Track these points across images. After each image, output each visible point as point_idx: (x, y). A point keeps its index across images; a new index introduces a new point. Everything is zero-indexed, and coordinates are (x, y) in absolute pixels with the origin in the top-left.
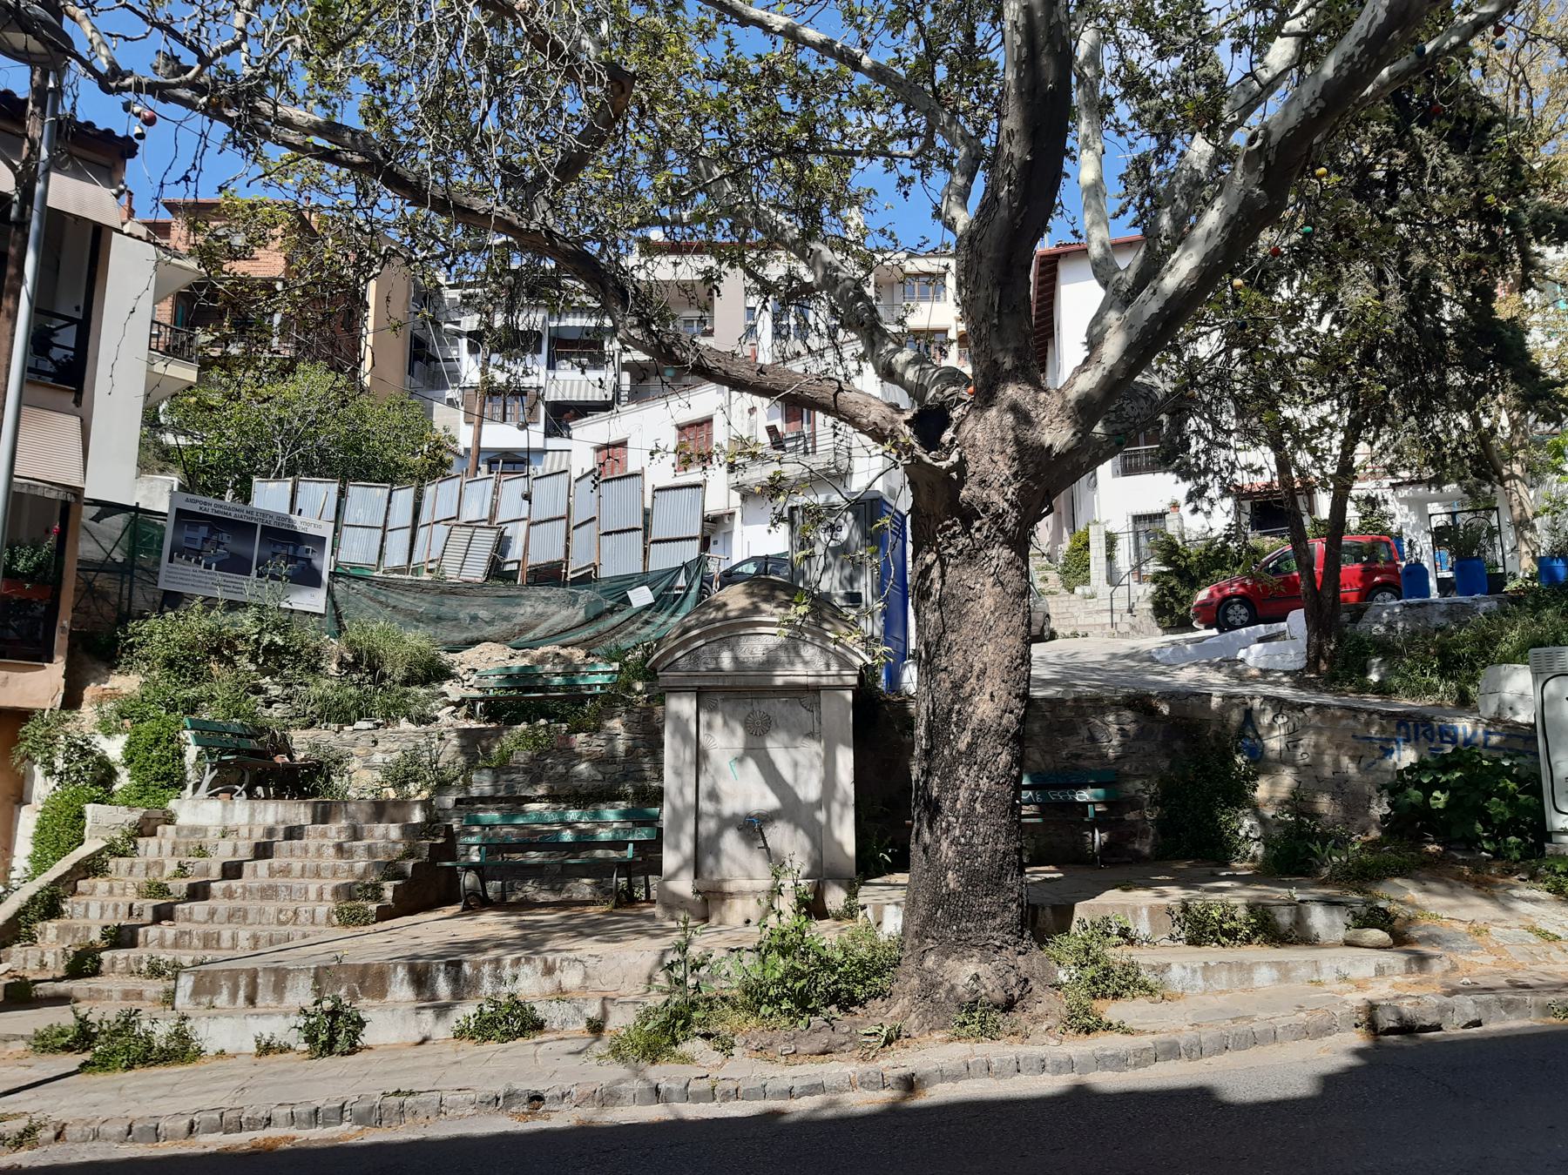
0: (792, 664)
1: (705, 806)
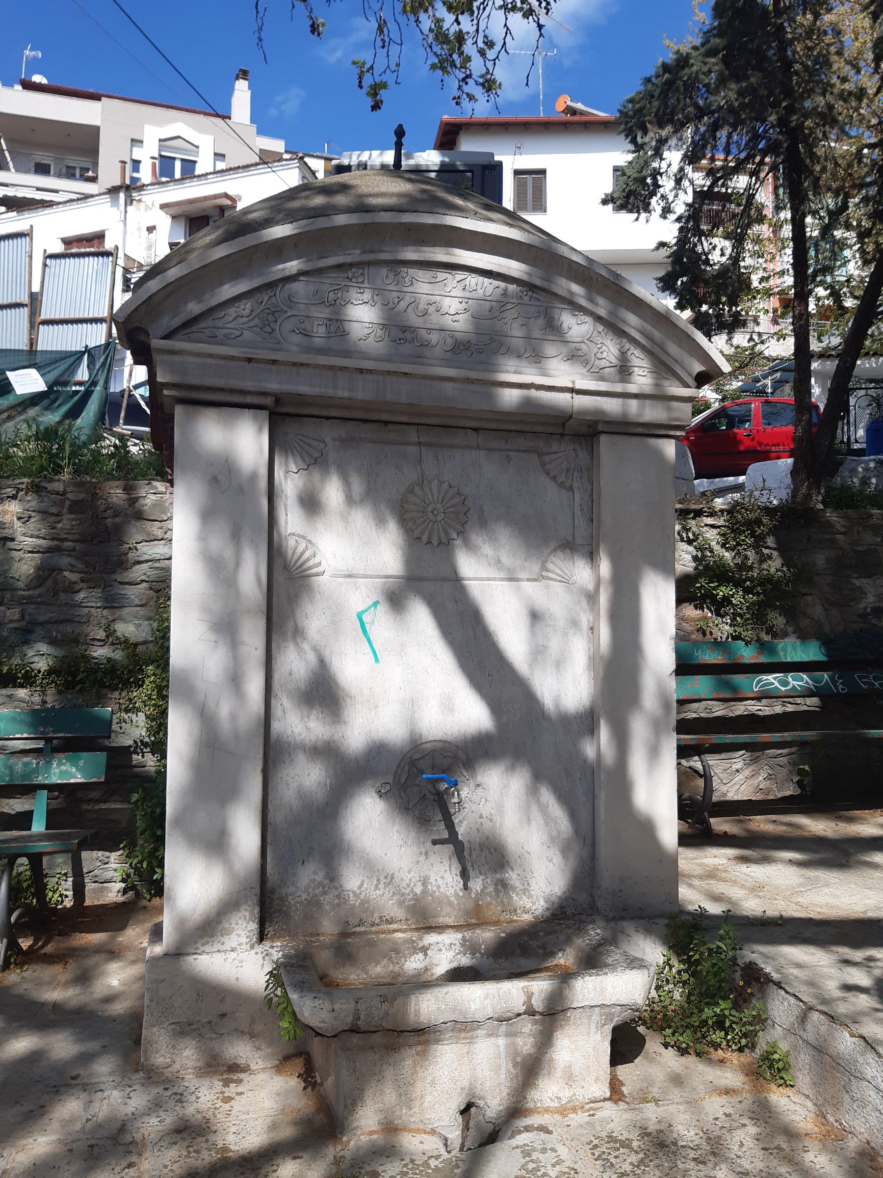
0: (537, 358)
1: (296, 724)
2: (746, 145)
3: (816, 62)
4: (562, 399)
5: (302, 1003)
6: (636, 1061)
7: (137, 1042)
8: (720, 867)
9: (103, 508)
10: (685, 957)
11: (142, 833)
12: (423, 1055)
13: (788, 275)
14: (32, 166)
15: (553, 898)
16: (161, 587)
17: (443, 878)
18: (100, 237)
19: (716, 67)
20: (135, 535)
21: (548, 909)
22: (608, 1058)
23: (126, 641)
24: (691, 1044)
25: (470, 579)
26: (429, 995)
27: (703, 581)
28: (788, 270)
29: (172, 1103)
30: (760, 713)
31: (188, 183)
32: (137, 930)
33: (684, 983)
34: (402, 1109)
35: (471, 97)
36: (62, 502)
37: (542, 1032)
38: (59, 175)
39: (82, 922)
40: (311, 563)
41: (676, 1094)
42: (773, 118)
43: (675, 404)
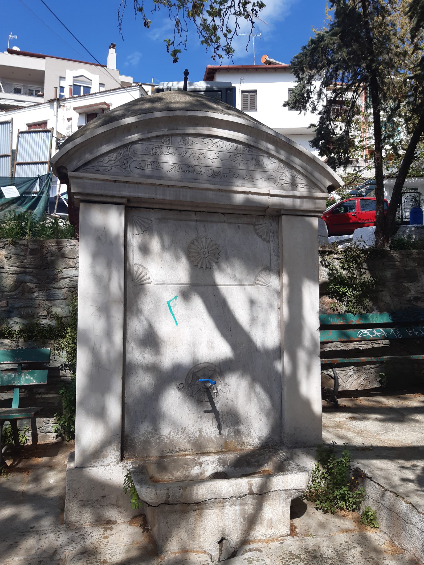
0: (252, 179)
1: (139, 356)
2: (351, 78)
3: (384, 39)
4: (264, 199)
5: (141, 490)
6: (303, 516)
7: (63, 510)
8: (342, 422)
9: (46, 252)
10: (326, 466)
11: (65, 409)
12: (200, 515)
13: (372, 139)
14: (12, 89)
15: (262, 438)
16: (73, 290)
17: (209, 429)
18: (45, 123)
19: (337, 41)
20: (61, 265)
21: (260, 443)
22: (289, 515)
23: (57, 316)
24: (329, 508)
25: (221, 285)
26: (203, 486)
27: (333, 285)
28: (372, 137)
29: (79, 539)
30: (361, 348)
31: (87, 98)
32: (63, 456)
33: (326, 478)
34: (190, 541)
35: (220, 56)
36: (26, 250)
37: (257, 503)
38: (25, 94)
39: (36, 452)
40: (145, 278)
41: (322, 532)
42: (364, 65)
43: (318, 201)
